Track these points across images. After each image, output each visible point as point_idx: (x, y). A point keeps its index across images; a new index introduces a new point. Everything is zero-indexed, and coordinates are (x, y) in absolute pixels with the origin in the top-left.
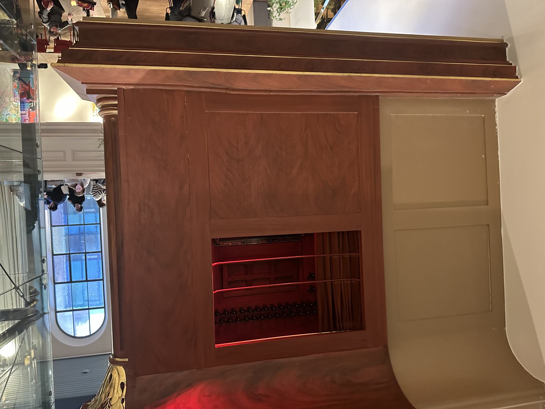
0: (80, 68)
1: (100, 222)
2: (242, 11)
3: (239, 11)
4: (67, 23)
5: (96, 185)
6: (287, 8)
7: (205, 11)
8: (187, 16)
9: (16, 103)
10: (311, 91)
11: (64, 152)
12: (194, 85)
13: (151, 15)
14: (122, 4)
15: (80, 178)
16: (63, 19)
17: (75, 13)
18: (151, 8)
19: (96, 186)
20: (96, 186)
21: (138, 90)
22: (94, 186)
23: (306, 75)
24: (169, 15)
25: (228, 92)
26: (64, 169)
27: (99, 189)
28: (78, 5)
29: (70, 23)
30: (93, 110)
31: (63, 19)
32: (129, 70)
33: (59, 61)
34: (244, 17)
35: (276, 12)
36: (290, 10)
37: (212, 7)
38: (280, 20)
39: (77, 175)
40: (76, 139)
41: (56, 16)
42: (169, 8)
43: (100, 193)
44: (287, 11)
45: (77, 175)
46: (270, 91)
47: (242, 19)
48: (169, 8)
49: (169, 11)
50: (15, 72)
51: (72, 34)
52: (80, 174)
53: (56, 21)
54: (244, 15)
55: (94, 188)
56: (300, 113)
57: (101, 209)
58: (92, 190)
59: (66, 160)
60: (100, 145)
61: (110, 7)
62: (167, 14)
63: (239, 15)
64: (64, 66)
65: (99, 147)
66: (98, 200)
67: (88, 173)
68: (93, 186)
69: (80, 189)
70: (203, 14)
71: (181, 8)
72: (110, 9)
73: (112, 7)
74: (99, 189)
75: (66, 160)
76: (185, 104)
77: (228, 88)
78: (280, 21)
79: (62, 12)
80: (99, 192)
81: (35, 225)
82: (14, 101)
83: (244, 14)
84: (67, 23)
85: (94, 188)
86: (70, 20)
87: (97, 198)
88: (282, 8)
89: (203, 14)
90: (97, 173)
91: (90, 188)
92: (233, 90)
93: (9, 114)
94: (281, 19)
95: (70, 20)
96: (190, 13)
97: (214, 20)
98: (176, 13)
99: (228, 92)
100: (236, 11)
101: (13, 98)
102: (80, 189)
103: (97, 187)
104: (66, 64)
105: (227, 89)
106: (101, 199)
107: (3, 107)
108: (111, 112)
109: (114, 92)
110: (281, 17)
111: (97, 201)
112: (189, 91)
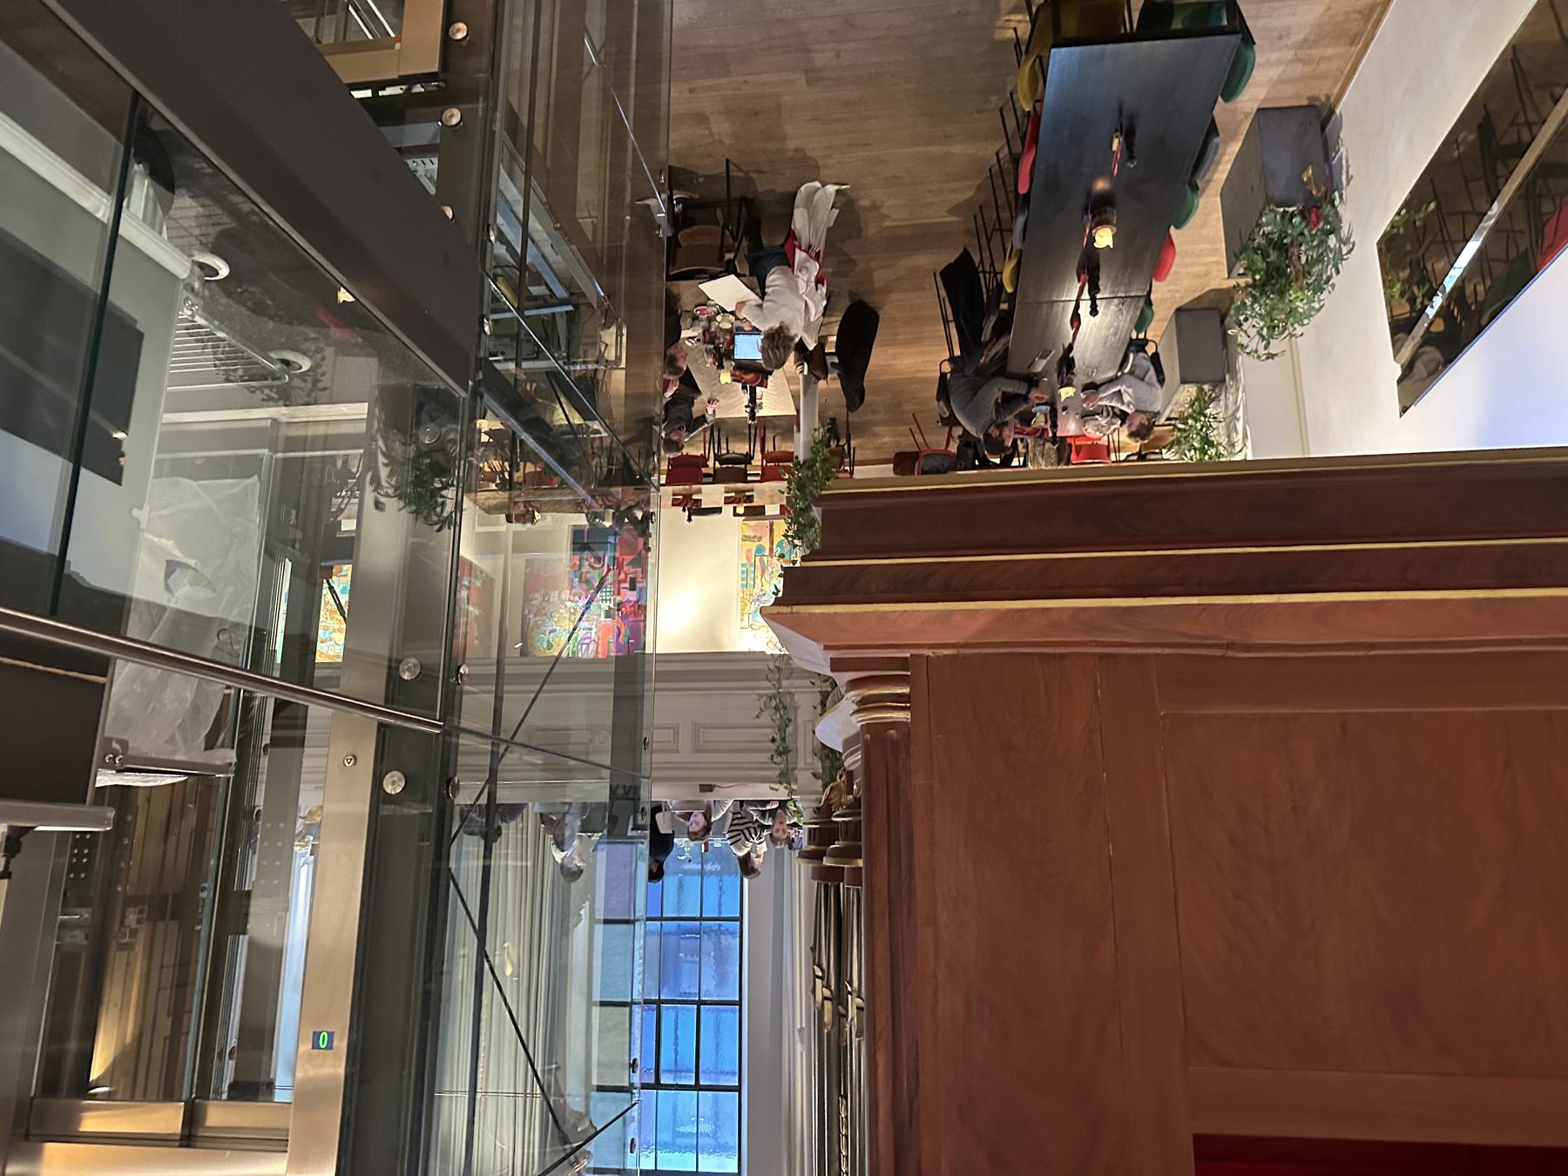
0: (829, 614)
1: (741, 914)
2: (1150, 343)
3: (1139, 345)
4: (703, 419)
5: (739, 813)
6: (1292, 325)
7: (1045, 358)
8: (994, 375)
9: (573, 604)
10: (1519, 642)
11: (675, 729)
12: (1127, 640)
13: (894, 377)
14: (833, 364)
15: (708, 798)
16: (696, 410)
17: (723, 398)
18: (898, 362)
19: (739, 816)
20: (739, 816)
21: (965, 657)
22: (735, 816)
23: (1505, 600)
24: (949, 375)
25: (1230, 654)
26: (672, 773)
27: (746, 823)
28: (733, 380)
29: (709, 418)
30: (742, 615)
31: (696, 410)
32: (952, 612)
33: (778, 602)
34: (1155, 359)
35: (1257, 337)
36: (1299, 330)
37: (1066, 346)
38: (1268, 358)
39: (701, 791)
40: (704, 695)
41: (682, 407)
42: (949, 360)
43: (748, 835)
44: (1290, 333)
45: (701, 791)
46: (1372, 646)
47: (1147, 364)
48: (949, 360)
49: (947, 368)
50: (577, 533)
51: (708, 438)
52: (706, 788)
53: (680, 418)
54: (1153, 354)
55: (735, 822)
56: (1479, 709)
57: (746, 881)
58: (731, 825)
59: (677, 751)
60: (762, 710)
61: (802, 372)
62: (943, 375)
63: (1141, 354)
64: (791, 613)
65: (758, 717)
66: (741, 854)
67: (727, 785)
68: (734, 814)
69: (697, 823)
70: (1040, 366)
71: (982, 361)
72: (801, 376)
73: (806, 373)
74: (746, 823)
75: (677, 751)
76: (1096, 691)
77: (1233, 644)
78: (1270, 360)
79: (694, 395)
80: (746, 831)
81: (582, 912)
82: (570, 600)
83: (1154, 351)
84: (703, 419)
85: (735, 822)
86: (710, 412)
87: (739, 849)
88: (1274, 328)
89: (1040, 366)
90: (751, 784)
91: (725, 822)
92: (1248, 648)
93: (555, 630)
94: (1271, 356)
95: (710, 412)
96: (1005, 367)
97: (1070, 379)
98: (969, 372)
99: (1230, 654)
100: (1132, 348)
101: (568, 592)
102: (697, 823)
103: (742, 818)
104: (796, 608)
105: (1229, 646)
106: (748, 854)
107: (545, 614)
108: (889, 715)
109: (903, 663)
110: (1272, 350)
111: (739, 858)
112: (1108, 656)
